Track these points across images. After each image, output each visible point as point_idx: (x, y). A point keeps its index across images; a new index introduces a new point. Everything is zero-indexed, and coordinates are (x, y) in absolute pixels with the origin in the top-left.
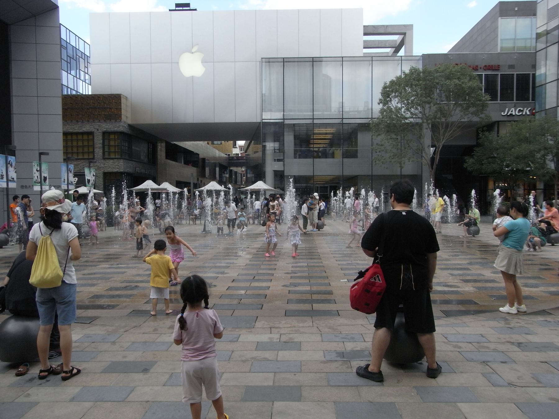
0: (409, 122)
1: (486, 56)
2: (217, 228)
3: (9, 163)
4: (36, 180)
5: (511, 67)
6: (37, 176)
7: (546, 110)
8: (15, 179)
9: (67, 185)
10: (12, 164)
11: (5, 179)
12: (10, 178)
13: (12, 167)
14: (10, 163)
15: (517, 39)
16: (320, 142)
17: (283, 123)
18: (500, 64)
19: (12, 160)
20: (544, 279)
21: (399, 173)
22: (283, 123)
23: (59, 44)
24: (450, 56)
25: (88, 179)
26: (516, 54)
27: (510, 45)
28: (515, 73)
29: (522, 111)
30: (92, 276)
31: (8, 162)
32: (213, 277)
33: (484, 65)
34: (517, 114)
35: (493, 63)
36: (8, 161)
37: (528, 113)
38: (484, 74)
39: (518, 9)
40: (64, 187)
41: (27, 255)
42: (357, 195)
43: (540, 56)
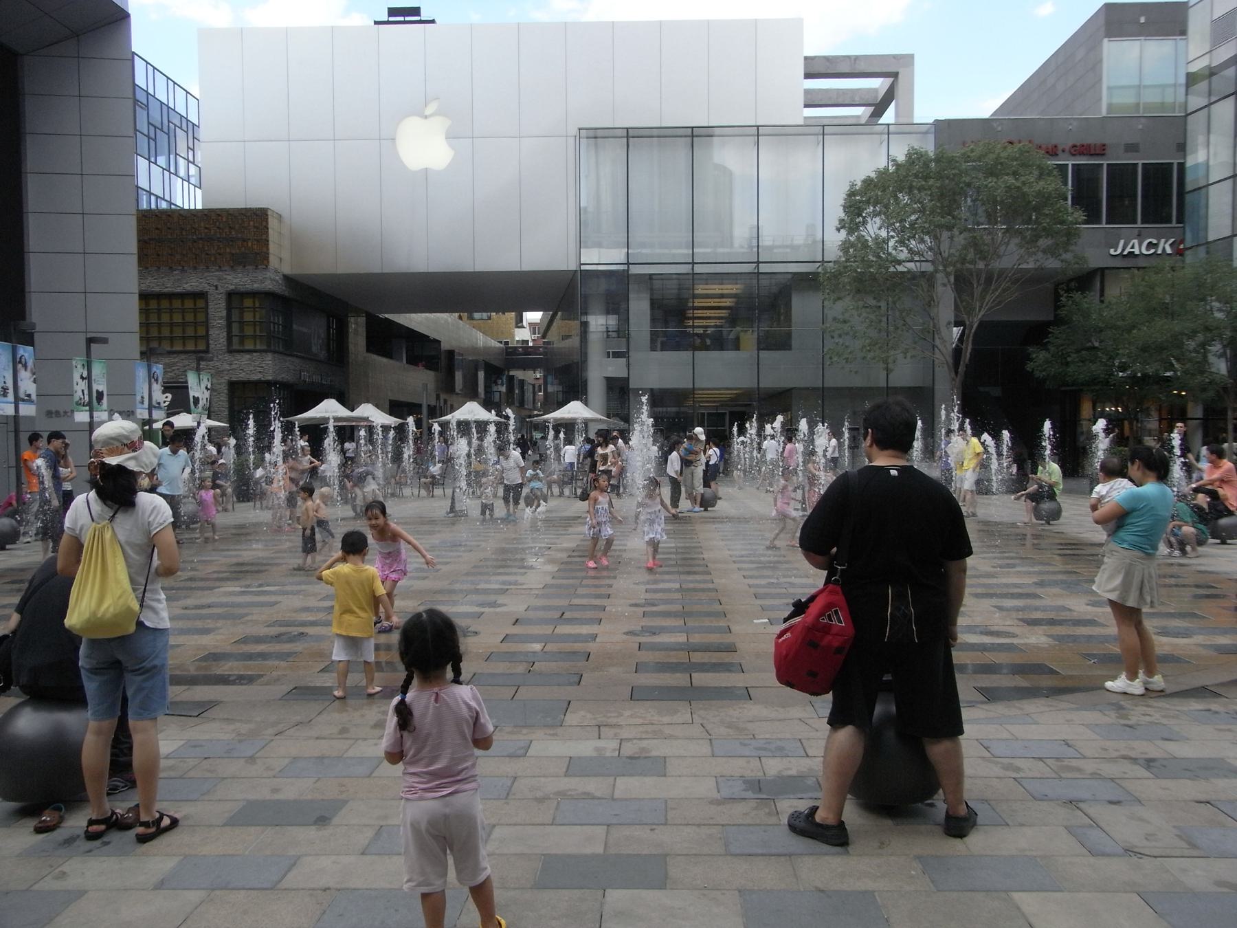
0: (906, 270)
1: (1075, 123)
2: (480, 505)
3: (20, 362)
4: (81, 399)
5: (1132, 148)
6: (83, 391)
7: (1208, 243)
8: (34, 397)
9: (147, 411)
10: (26, 363)
11: (11, 397)
12: (22, 395)
13: (26, 370)
14: (23, 360)
15: (1145, 87)
16: (708, 315)
17: (626, 273)
18: (1106, 141)
19: (26, 355)
20: (1204, 617)
21: (883, 384)
22: (626, 273)
23: (131, 97)
24: (995, 125)
25: (194, 397)
26: (1143, 120)
27: (1128, 99)
28: (1140, 162)
29: (1156, 246)
30: (204, 612)
31: (18, 360)
32: (471, 613)
33: (1070, 143)
34: (1145, 252)
35: (1092, 139)
36: (19, 356)
37: (1169, 250)
38: (1070, 163)
39: (1146, 19)
40: (141, 414)
41: (60, 565)
42: (790, 433)
43: (1196, 125)
